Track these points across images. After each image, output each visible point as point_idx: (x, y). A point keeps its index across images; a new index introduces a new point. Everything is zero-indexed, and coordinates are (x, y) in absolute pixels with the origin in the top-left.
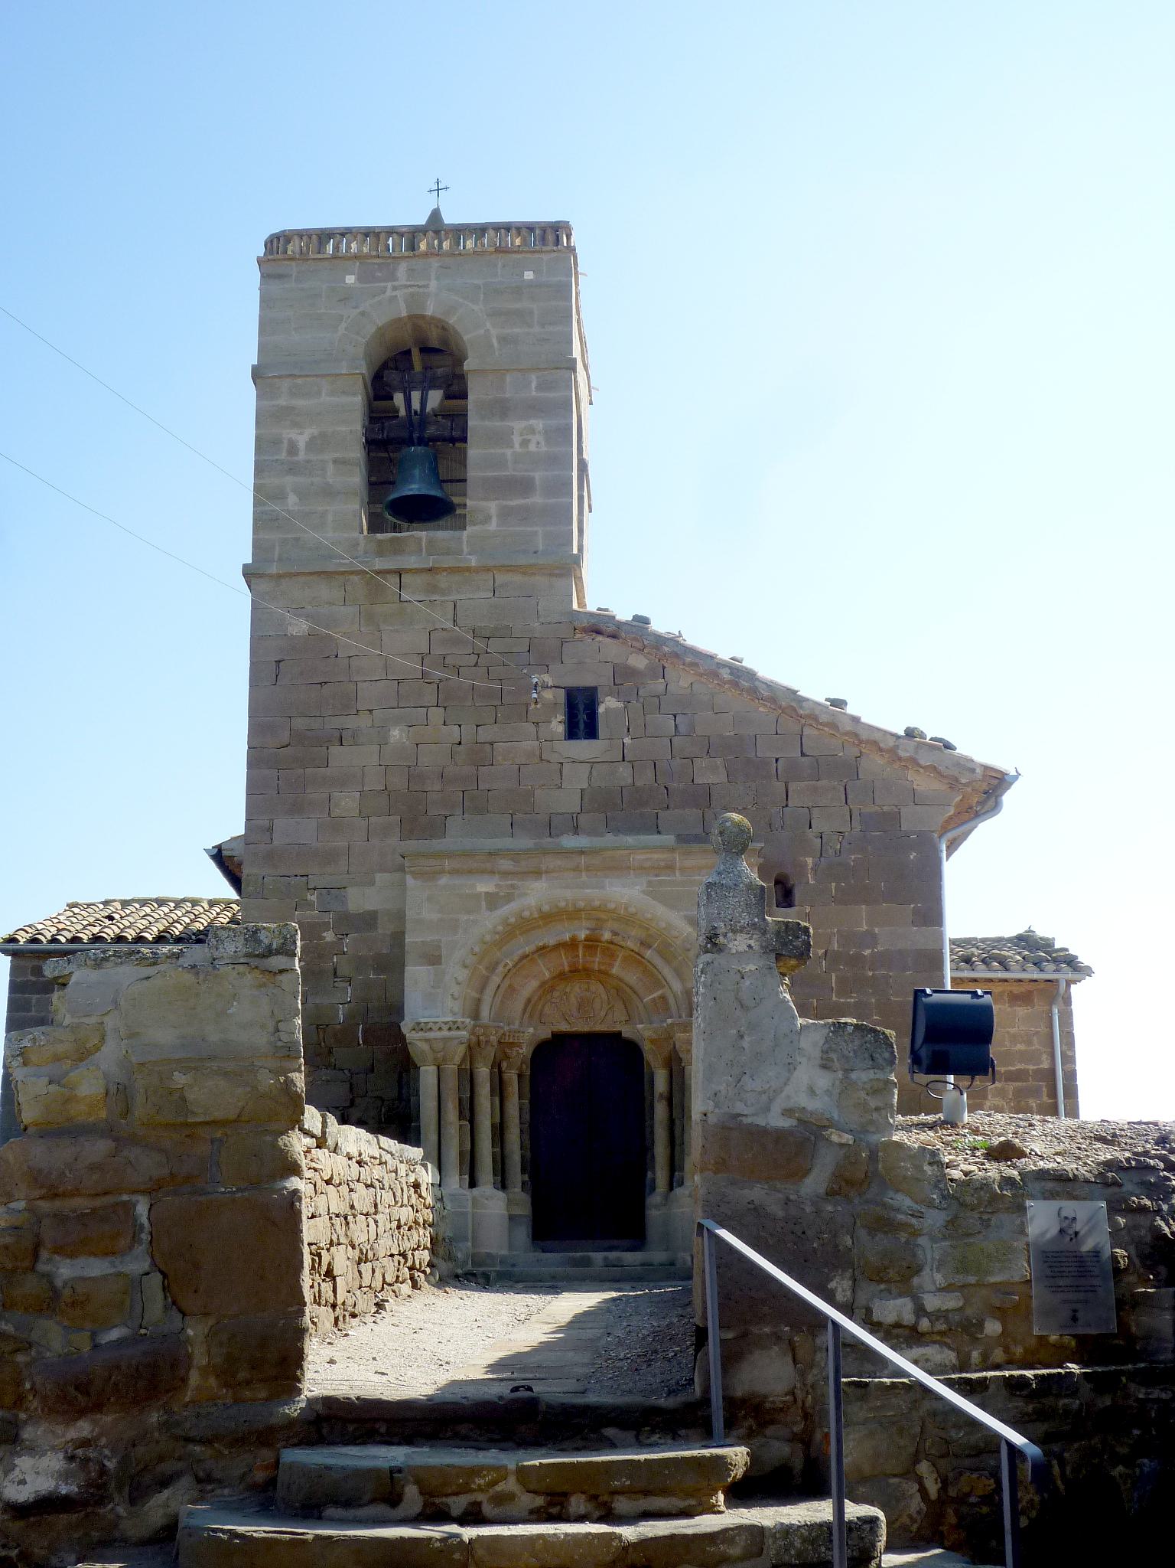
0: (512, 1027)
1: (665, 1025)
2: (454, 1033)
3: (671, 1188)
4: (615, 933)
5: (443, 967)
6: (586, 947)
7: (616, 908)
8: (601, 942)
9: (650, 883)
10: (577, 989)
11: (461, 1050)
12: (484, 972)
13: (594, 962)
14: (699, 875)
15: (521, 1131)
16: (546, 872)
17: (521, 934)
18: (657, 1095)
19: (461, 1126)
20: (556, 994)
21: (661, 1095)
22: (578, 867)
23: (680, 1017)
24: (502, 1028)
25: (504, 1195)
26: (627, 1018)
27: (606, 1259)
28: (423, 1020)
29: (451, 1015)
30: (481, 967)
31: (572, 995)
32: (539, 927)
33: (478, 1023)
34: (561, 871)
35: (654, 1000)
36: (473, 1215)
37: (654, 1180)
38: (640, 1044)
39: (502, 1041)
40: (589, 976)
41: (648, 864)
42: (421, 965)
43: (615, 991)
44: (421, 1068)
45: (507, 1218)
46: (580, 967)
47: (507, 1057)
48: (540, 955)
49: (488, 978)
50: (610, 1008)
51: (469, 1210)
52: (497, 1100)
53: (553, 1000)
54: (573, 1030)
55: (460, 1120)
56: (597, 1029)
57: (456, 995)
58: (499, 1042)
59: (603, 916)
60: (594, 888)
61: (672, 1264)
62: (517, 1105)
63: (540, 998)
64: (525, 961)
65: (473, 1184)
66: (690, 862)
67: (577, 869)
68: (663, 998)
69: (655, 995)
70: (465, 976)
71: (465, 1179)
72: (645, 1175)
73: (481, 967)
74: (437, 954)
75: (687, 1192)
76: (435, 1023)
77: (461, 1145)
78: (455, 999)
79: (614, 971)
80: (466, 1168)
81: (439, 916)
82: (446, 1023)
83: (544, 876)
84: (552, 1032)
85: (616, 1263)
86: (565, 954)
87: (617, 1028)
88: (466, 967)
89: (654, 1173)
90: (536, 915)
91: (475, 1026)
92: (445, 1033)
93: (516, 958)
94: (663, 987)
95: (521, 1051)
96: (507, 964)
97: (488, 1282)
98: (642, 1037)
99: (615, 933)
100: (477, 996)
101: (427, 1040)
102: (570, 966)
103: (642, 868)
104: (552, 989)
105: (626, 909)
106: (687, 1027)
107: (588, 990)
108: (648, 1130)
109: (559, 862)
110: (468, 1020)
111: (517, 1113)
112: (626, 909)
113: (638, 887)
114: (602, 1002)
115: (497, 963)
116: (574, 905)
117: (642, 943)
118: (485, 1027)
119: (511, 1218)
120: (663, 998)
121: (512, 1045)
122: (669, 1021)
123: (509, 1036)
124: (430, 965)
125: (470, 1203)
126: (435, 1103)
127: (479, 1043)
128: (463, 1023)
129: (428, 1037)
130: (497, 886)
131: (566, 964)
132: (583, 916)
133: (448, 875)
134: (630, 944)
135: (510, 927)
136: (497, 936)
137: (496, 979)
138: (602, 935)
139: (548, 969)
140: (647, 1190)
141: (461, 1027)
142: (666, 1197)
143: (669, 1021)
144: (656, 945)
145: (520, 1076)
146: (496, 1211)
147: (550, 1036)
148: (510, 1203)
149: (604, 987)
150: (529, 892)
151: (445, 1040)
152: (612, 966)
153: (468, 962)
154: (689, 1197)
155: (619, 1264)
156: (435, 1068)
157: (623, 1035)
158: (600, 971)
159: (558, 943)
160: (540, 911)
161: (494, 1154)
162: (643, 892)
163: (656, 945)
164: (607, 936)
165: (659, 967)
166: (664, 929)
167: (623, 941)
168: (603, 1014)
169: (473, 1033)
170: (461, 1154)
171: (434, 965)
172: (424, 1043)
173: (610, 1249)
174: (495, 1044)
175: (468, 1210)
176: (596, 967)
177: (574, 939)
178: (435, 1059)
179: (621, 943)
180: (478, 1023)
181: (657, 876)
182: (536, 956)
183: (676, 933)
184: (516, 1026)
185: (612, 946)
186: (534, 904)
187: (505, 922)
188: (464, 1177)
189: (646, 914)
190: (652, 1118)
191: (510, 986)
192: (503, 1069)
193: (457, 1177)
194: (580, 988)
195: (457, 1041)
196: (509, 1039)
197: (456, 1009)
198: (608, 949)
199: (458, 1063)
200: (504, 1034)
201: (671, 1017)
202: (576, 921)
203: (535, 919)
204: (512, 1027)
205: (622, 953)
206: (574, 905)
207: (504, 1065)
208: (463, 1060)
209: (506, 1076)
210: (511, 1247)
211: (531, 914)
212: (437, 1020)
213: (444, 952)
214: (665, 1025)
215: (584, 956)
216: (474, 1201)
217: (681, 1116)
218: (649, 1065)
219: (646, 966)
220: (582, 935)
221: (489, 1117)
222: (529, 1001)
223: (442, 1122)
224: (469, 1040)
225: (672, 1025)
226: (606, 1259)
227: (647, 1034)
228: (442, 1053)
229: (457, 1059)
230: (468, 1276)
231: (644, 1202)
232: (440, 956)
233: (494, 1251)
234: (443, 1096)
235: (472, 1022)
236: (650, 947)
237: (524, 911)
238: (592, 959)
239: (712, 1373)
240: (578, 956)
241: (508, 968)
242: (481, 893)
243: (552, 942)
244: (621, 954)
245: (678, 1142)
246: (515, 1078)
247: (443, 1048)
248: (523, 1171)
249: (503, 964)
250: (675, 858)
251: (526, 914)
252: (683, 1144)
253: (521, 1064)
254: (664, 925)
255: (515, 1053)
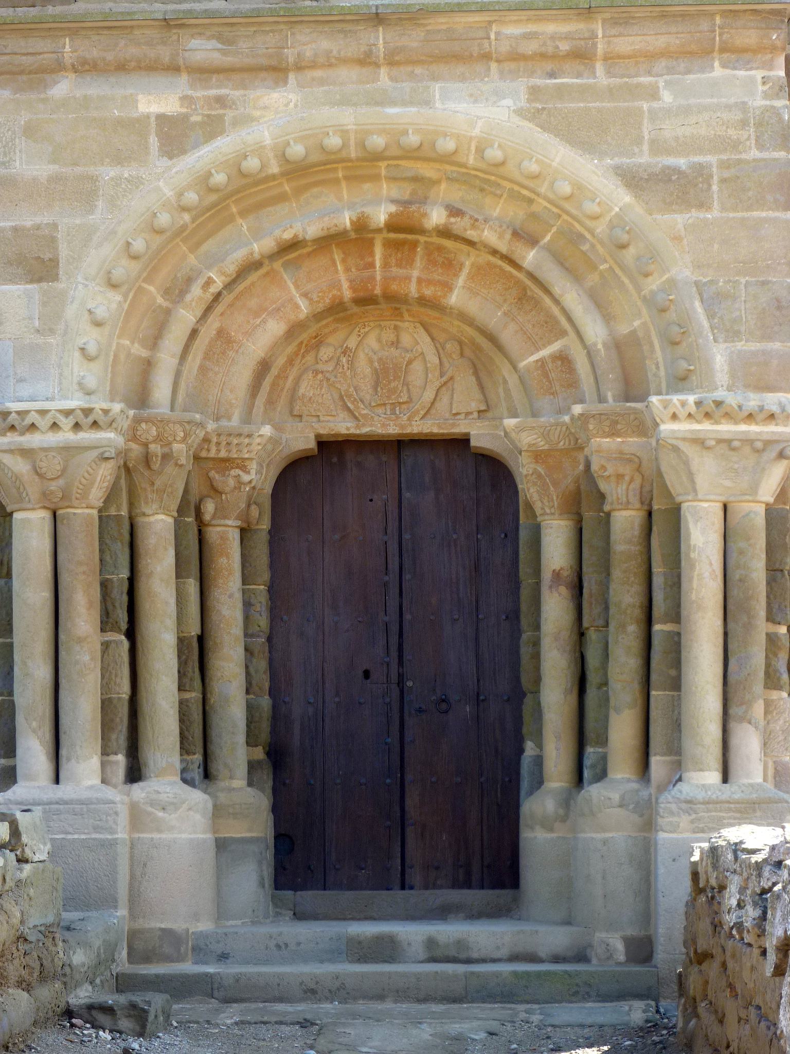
0: (224, 423)
1: (567, 418)
2: (87, 436)
3: (579, 780)
4: (454, 212)
5: (61, 285)
6: (388, 244)
7: (456, 152)
8: (422, 231)
9: (535, 93)
10: (372, 341)
11: (105, 474)
12: (160, 300)
13: (408, 278)
14: (649, 73)
15: (246, 649)
16: (299, 68)
17: (243, 213)
18: (546, 576)
19: (106, 646)
20: (326, 352)
21: (557, 575)
22: (369, 54)
23: (601, 399)
24: (201, 425)
25: (206, 797)
26: (483, 408)
27: (431, 943)
28: (14, 406)
29: (79, 394)
30: (151, 288)
31: (361, 356)
32: (282, 198)
33: (145, 413)
34: (331, 65)
35: (542, 362)
36: (132, 847)
37: (539, 761)
38: (511, 464)
39: (204, 454)
40: (397, 314)
41: (531, 47)
42: (12, 281)
43: (456, 344)
44: (15, 515)
45: (212, 845)
46: (378, 291)
47: (215, 491)
48: (286, 265)
49: (168, 312)
50: (445, 383)
51: (122, 834)
52: (192, 587)
53: (320, 367)
54: (365, 430)
55: (102, 630)
56: (416, 430)
57: (92, 349)
58: (197, 458)
59: (428, 171)
60: (405, 104)
61: (581, 957)
62: (238, 596)
63: (290, 362)
64: (253, 277)
65: (134, 774)
66: (627, 43)
67: (366, 60)
68: (563, 359)
69: (545, 352)
70: (114, 306)
71: (117, 763)
72: (521, 751)
73: (151, 288)
74: (47, 256)
75: (616, 797)
76: (43, 413)
77: (106, 685)
78: (90, 359)
79: (455, 299)
80: (120, 737)
81: (54, 168)
82: (68, 413)
83: (292, 76)
84: (318, 436)
85: (453, 953)
86: (344, 261)
87: (460, 428)
88: (114, 286)
89: (540, 745)
90: (274, 169)
91: (137, 421)
92: (67, 436)
93: (231, 268)
94: (564, 333)
95: (246, 478)
96: (209, 282)
97: (144, 1026)
98: (516, 447)
99: (454, 212)
100: (144, 353)
101: (26, 453)
102: (353, 288)
103: (516, 57)
104: (318, 342)
105: (480, 151)
106: (617, 422)
107: (396, 344)
108: (525, 651)
109: (325, 44)
110: (117, 407)
111: (239, 615)
112: (480, 151)
113: (508, 102)
114: (427, 369)
115: (189, 281)
116: (362, 145)
117: (516, 234)
118: (160, 422)
119: (221, 845)
120: (563, 359)
121: (225, 464)
122: (577, 409)
123: (218, 444)
124: (31, 281)
125: (123, 819)
126: (46, 595)
127: (147, 460)
128: (106, 412)
129: (26, 446)
130: (184, 98)
131: (345, 285)
132: (383, 172)
133: (72, 76)
134: (489, 236)
135: (213, 197)
136: (187, 217)
137: (186, 317)
138: (425, 215)
139: (305, 295)
140: (525, 785)
141: (101, 423)
142: (567, 802)
143: (577, 409)
144: (548, 238)
145: (245, 532)
146: (184, 836)
147: (312, 444)
148: (218, 812)
149: (433, 339)
150: (257, 113)
151: (68, 450)
152: (448, 287)
153: (118, 274)
154: (621, 806)
155: (463, 956)
156: (46, 515)
157: (473, 443)
158: (422, 301)
159: (325, 233)
160: (283, 157)
161: (183, 705)
162: (519, 112)
163: (548, 238)
164: (436, 217)
165: (557, 290)
166: (567, 198)
167: (473, 227)
168: (429, 395)
169: (133, 436)
170: (106, 705)
171: (40, 280)
172: (19, 459)
173: (442, 913)
174: (183, 461)
175: (120, 836)
176: (413, 290)
177: (361, 226)
178: (45, 495)
179: (471, 234)
180: (145, 413)
181: (552, 75)
182: (277, 265)
183: (592, 208)
184: (235, 422)
185: (448, 244)
186: (268, 141)
187: (203, 182)
188: (113, 758)
189: (526, 163)
190: (537, 627)
191: (220, 332)
192: (207, 517)
193: (95, 762)
194: (379, 340)
195: (95, 453)
196: (219, 451)
197: (91, 382)
198: (440, 249)
199: (100, 504)
200: (206, 440)
201: (582, 401)
202: (367, 186)
203: (273, 177)
204: (224, 423)
205: (472, 259)
206: (362, 145)
207: (209, 507)
208: (111, 497)
209: (213, 534)
210: (221, 912)
211: (263, 167)
212: (46, 405)
213: (64, 251)
214: (567, 418)
215: (386, 265)
216: (137, 817)
217: (601, 622)
218: (529, 507)
219: (525, 289)
220: (381, 215)
221: (171, 622)
222: (264, 367)
223: (62, 637)
224: (123, 454)
225: (584, 418)
226: (431, 943)
227: (526, 439)
228: (61, 482)
229: (97, 495)
230: (94, 1013)
231: (517, 806)
232: (55, 262)
233: (178, 925)
234: (64, 578)
235: (131, 413)
236: (533, 241)
237: (245, 157)
238: (401, 272)
239: (522, 556)
240: (372, 265)
241: (213, 289)
242: (148, 116)
243: (313, 230)
244: (469, 260)
245: (593, 678)
246: (234, 536)
247: (64, 470)
248: (251, 741)
249: (201, 281)
250: (593, 36)
251: (252, 164)
252: (606, 684)
253: (249, 506)
254: (565, 188)
255: (231, 482)
